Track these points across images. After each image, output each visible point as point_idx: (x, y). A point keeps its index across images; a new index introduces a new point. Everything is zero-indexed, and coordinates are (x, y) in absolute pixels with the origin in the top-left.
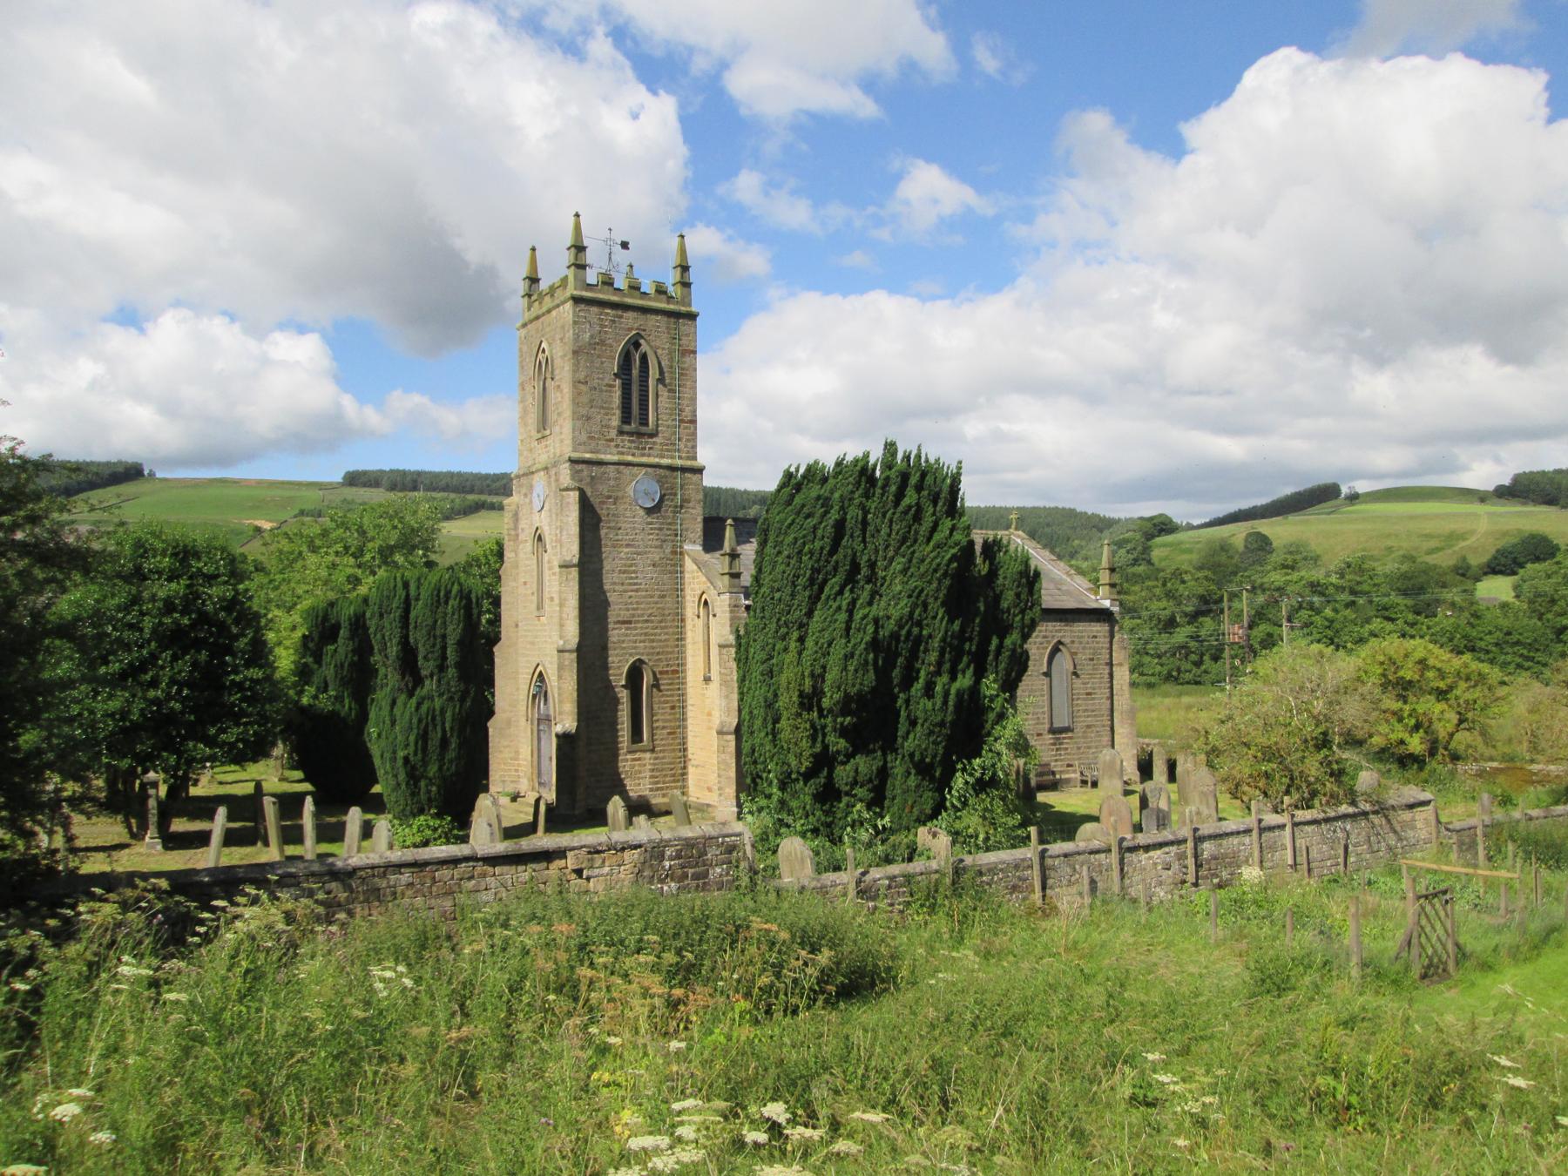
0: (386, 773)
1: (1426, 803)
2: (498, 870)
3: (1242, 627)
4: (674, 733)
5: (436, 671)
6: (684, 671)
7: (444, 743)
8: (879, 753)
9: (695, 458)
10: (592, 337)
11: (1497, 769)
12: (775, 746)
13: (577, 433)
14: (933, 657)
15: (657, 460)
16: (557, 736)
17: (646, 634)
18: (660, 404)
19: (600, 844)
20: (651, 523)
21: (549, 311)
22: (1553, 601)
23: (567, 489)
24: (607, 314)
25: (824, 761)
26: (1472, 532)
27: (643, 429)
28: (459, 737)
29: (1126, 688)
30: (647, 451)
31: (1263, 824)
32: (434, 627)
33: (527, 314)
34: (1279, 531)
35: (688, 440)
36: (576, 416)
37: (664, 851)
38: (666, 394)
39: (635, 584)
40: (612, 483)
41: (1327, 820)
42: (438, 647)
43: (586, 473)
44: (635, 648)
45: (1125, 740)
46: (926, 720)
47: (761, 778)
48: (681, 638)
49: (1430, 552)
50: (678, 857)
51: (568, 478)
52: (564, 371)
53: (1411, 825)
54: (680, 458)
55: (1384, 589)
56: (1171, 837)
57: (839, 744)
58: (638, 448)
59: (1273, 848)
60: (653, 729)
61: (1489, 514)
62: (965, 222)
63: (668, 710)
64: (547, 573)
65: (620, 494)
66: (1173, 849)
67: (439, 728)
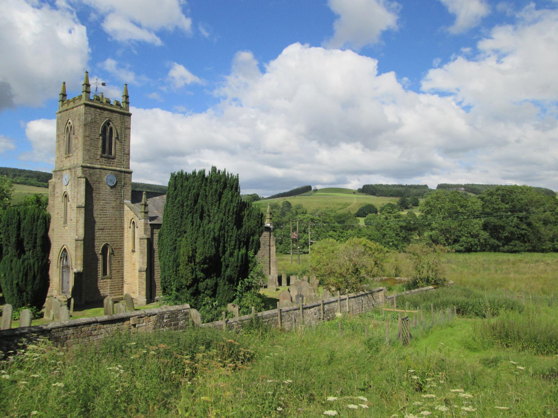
0: (8, 290)
1: (381, 290)
2: (105, 326)
3: (296, 233)
4: (119, 272)
5: (32, 248)
6: (123, 248)
7: (34, 277)
8: (215, 278)
9: (129, 168)
10: (91, 119)
11: (386, 279)
12: (177, 276)
13: (85, 156)
14: (233, 243)
15: (115, 168)
16: (75, 273)
17: (109, 234)
18: (116, 147)
19: (142, 314)
20: (112, 192)
21: (73, 108)
22: (382, 226)
23: (80, 177)
24: (97, 111)
25: (196, 281)
26: (352, 203)
27: (110, 156)
28: (41, 275)
29: (275, 254)
30: (111, 165)
31: (341, 299)
32: (32, 230)
33: (61, 108)
34: (294, 201)
35: (127, 161)
36: (84, 149)
37: (164, 316)
38: (119, 143)
39: (106, 215)
40: (98, 176)
41: (358, 296)
42: (33, 238)
43: (88, 171)
44: (105, 239)
45: (274, 272)
46: (232, 265)
47: (168, 288)
48: (122, 236)
49: (339, 209)
50: (169, 318)
51: (81, 173)
52: (80, 132)
53: (378, 297)
54: (123, 168)
55: (333, 221)
56: (316, 304)
57: (201, 275)
58: (108, 163)
59: (343, 306)
60: (111, 270)
61: (357, 198)
62: (193, 87)
63: (117, 263)
64: (69, 210)
65: (101, 180)
66: (317, 308)
67: (32, 271)
